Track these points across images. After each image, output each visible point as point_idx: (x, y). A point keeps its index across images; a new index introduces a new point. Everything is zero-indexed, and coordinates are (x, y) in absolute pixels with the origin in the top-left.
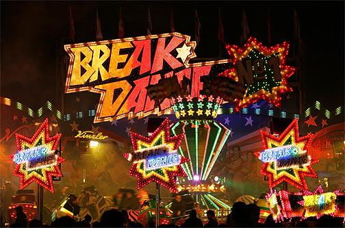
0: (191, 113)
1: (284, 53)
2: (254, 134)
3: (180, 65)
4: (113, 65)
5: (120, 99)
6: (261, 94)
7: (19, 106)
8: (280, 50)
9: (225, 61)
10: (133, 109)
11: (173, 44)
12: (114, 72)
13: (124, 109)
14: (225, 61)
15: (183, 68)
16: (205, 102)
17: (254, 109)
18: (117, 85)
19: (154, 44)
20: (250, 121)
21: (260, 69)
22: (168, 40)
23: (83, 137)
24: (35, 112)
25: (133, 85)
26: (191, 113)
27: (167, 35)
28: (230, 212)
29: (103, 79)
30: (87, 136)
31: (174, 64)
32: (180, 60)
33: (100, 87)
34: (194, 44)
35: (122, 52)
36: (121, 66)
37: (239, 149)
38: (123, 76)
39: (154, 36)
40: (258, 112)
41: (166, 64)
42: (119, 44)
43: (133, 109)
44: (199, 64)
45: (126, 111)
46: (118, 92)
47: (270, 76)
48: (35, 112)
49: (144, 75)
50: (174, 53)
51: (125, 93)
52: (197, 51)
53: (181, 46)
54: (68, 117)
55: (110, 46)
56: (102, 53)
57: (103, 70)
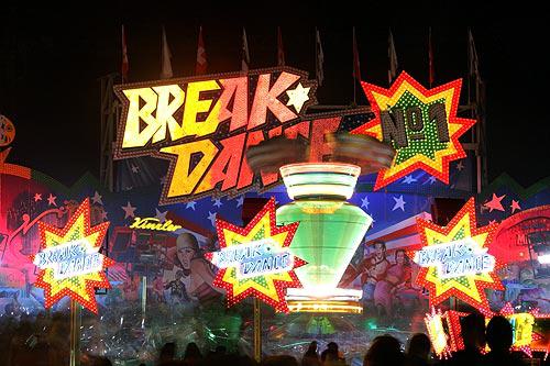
4: (189, 116)
5: (200, 169)
12: (191, 126)
18: (195, 147)
23: (143, 227)
25: (220, 147)
32: (292, 108)
35: (204, 96)
37: (384, 247)
46: (196, 158)
50: (283, 98)
51: (207, 159)
56: (171, 98)
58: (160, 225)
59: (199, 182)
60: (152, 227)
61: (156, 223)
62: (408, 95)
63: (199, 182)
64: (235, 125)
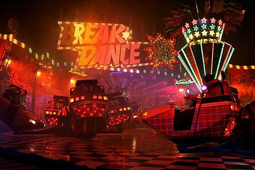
0: (197, 34)
1: (173, 43)
2: (158, 84)
3: (124, 41)
4: (87, 36)
5: (90, 56)
6: (164, 62)
7: (30, 51)
8: (172, 42)
9: (146, 43)
10: (98, 63)
11: (120, 30)
12: (87, 40)
13: (93, 63)
14: (146, 43)
15: (125, 43)
16: (209, 24)
17: (157, 72)
18: (88, 48)
19: (110, 28)
20: (155, 77)
21: (163, 49)
22: (118, 27)
23: (180, 83)
24: (40, 57)
25: (98, 49)
26: (197, 34)
27: (116, 25)
28: (98, 69)
29: (81, 43)
30: (182, 83)
31: (121, 41)
32: (124, 39)
33: (79, 48)
34: (131, 32)
35: (92, 30)
36: (91, 37)
37: (149, 92)
38: (92, 43)
39: (110, 25)
40: (159, 73)
41: (116, 40)
42: (90, 25)
43: (98, 63)
44: (134, 43)
45: (94, 63)
46: (89, 52)
47: (168, 54)
48: (40, 57)
49: (104, 44)
50: (121, 35)
51: (94, 52)
52: (132, 35)
53: (124, 31)
54: (58, 64)
55: (85, 26)
56: (80, 29)
57: (81, 38)
58: (186, 82)
59: (90, 61)
60: (184, 83)
61: (185, 81)
62: (222, 44)
63: (90, 61)
64: (104, 41)
